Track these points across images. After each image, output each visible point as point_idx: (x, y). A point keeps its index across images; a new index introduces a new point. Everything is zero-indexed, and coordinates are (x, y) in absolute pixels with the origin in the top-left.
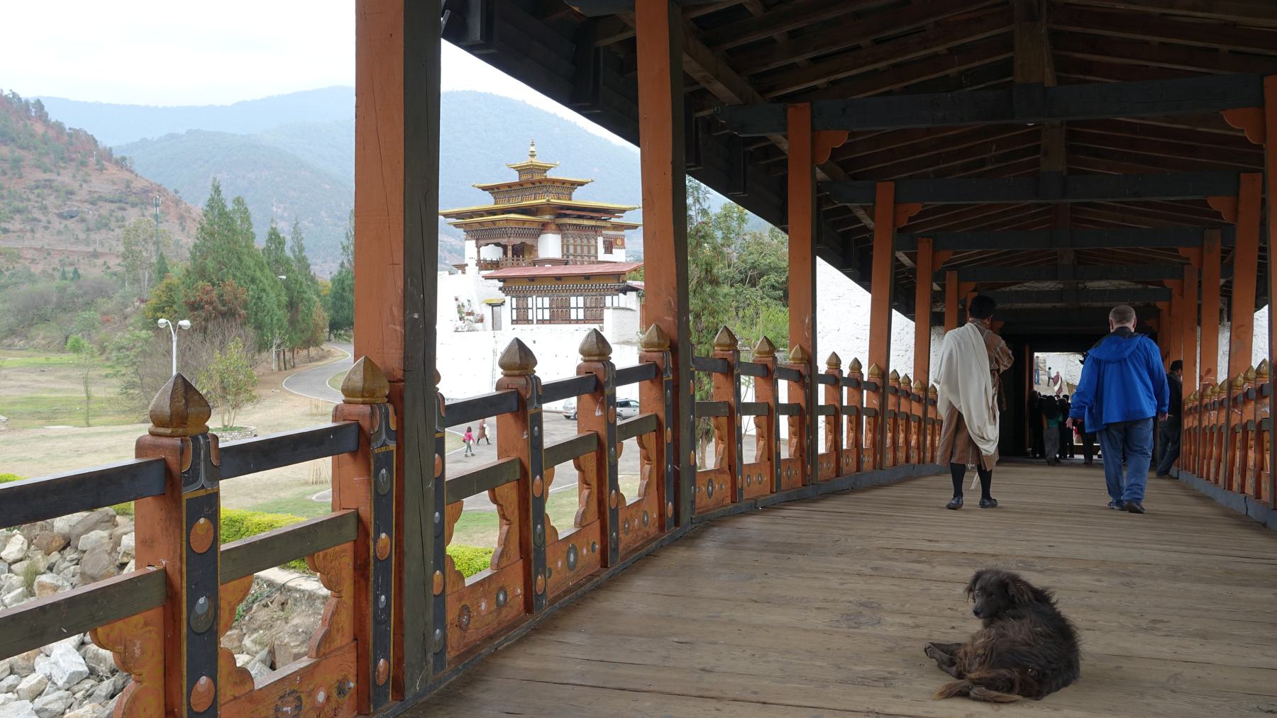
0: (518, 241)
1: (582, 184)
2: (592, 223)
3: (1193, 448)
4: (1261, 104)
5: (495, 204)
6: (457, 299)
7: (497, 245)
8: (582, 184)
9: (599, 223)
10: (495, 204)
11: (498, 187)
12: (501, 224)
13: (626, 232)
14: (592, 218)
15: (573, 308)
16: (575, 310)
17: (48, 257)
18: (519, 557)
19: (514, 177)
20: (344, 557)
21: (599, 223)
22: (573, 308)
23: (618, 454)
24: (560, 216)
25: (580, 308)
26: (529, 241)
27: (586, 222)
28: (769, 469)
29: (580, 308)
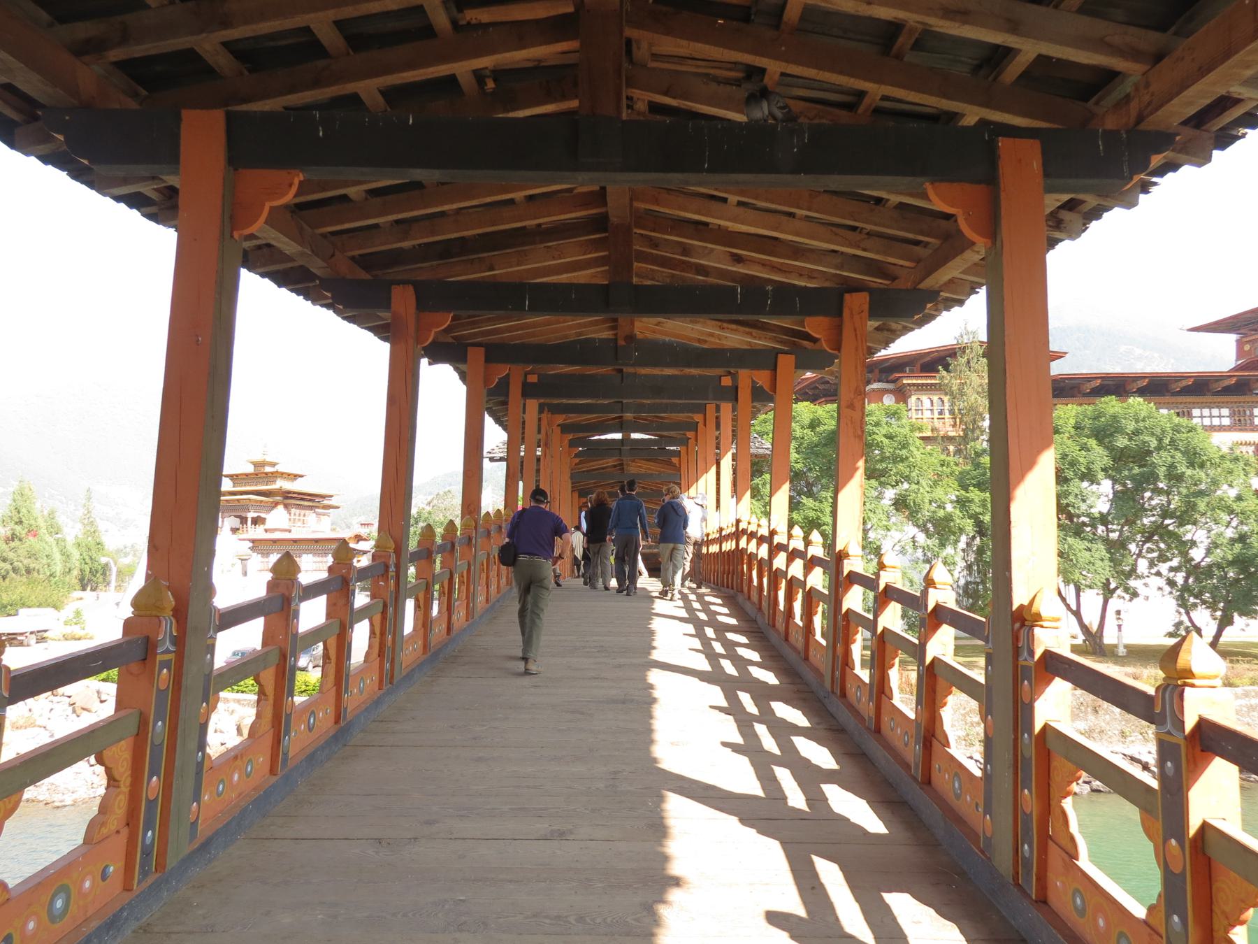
0: (255, 515)
1: (301, 476)
2: (310, 504)
3: (731, 568)
4: (775, 369)
5: (234, 487)
6: (106, 531)
7: (236, 517)
8: (301, 476)
9: (314, 504)
10: (234, 487)
11: (237, 475)
12: (242, 503)
13: (331, 510)
14: (310, 500)
15: (1211, 422)
16: (1213, 415)
17: (889, 533)
18: (270, 725)
19: (250, 469)
20: (121, 752)
21: (314, 504)
22: (1211, 422)
23: (367, 655)
24: (287, 498)
25: (1202, 413)
26: (263, 515)
27: (306, 503)
28: (1011, 770)
29: (1202, 413)
